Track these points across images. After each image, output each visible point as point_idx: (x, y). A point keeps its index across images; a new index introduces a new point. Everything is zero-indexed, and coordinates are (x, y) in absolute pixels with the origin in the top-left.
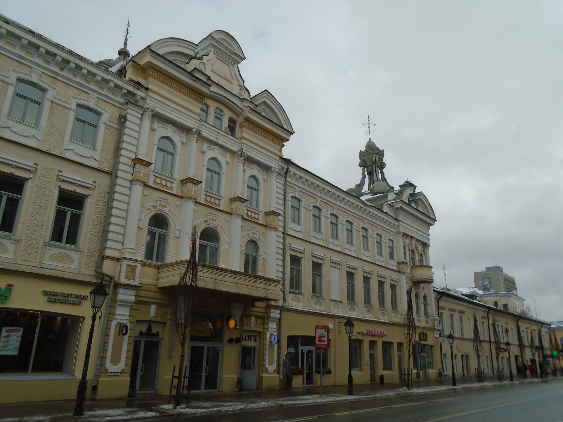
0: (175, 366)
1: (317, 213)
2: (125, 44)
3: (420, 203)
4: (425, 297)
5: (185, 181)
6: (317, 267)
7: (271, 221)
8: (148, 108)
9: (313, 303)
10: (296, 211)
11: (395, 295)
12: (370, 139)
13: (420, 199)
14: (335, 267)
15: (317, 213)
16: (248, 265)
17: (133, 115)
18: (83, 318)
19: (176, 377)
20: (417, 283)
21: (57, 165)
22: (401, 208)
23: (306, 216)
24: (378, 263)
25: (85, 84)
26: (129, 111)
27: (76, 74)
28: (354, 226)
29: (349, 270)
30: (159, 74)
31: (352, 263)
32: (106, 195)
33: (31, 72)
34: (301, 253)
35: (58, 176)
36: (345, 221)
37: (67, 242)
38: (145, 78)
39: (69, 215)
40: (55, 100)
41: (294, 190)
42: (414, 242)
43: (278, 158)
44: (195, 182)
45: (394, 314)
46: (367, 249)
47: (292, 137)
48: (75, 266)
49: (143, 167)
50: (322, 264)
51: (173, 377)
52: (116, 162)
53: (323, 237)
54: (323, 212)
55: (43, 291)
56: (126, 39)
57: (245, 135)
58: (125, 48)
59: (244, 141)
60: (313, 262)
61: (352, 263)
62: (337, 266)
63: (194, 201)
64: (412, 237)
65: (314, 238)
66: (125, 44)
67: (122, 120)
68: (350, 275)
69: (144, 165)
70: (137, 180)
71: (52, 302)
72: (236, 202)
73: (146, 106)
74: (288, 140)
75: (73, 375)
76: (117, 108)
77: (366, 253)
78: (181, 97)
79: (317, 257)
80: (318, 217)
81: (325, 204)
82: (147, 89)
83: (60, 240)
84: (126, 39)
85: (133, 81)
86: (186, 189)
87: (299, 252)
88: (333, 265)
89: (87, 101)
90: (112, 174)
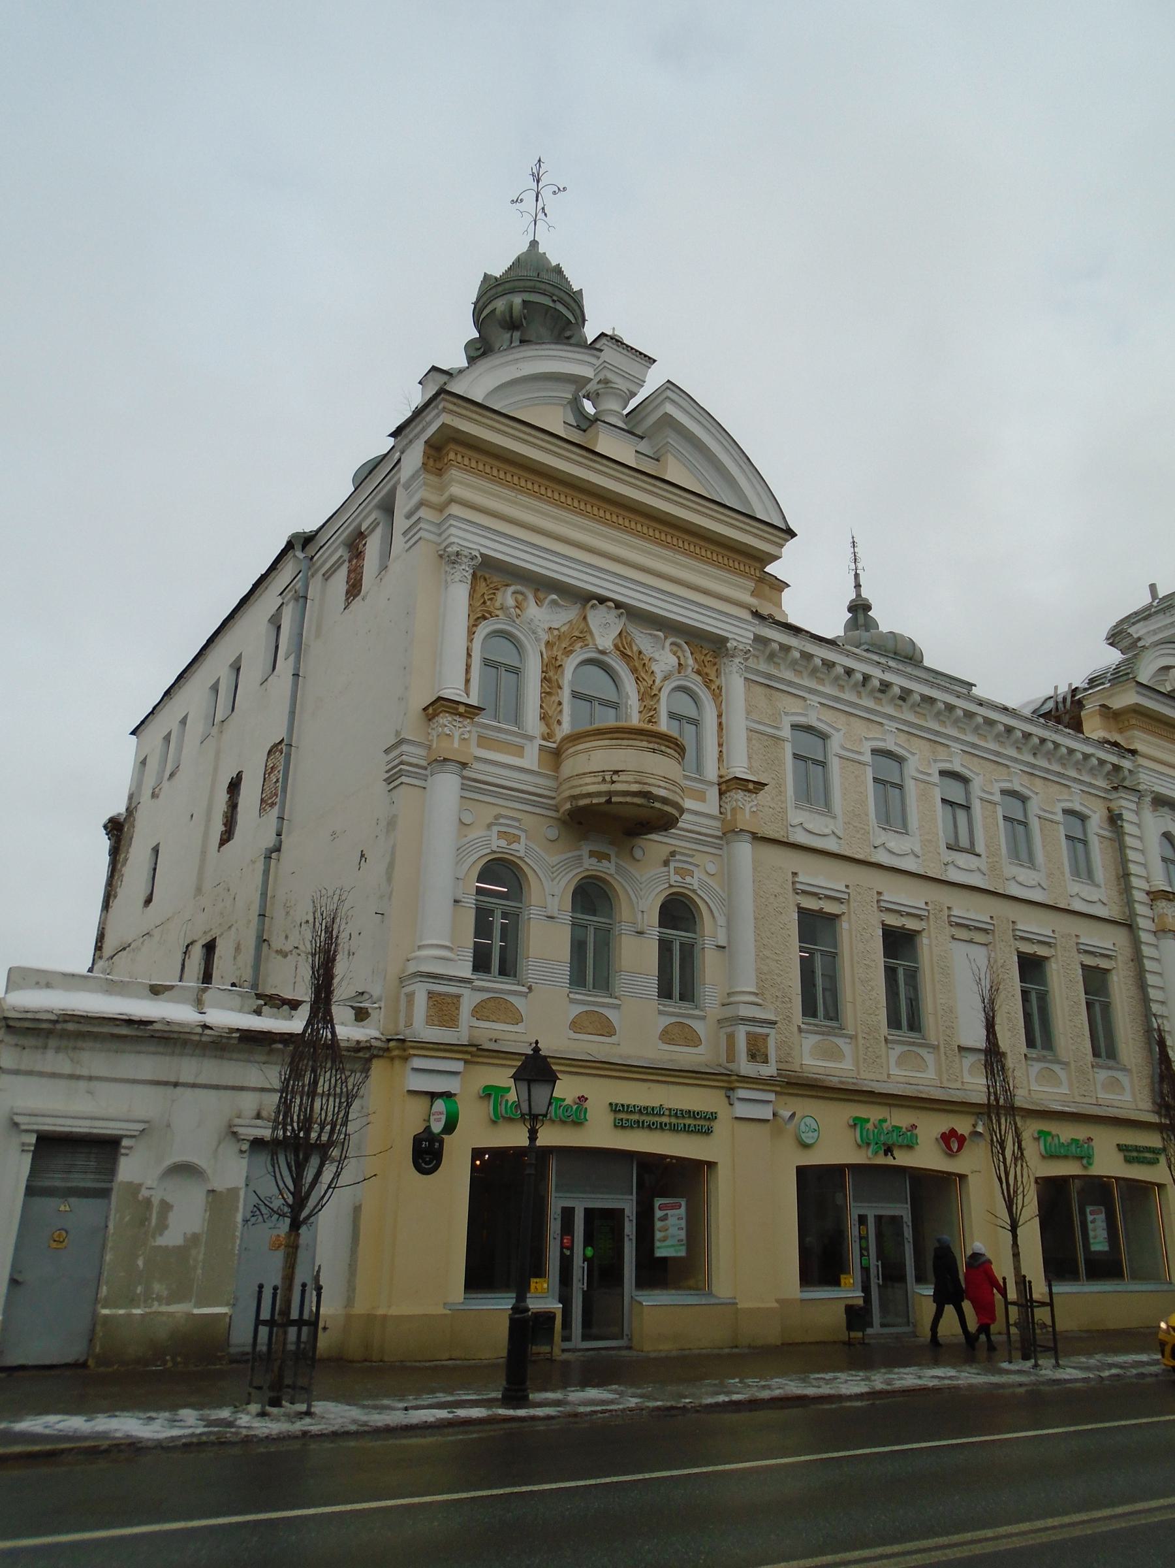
0: (261, 1287)
1: (956, 792)
2: (858, 586)
3: (673, 439)
4: (678, 912)
5: (430, 710)
6: (899, 942)
7: (733, 810)
8: (458, 554)
9: (893, 1061)
10: (961, 815)
11: (1043, 998)
12: (534, 244)
13: (668, 421)
14: (971, 941)
15: (956, 792)
16: (1039, 1008)
17: (1125, 804)
18: (711, 1165)
19: (265, 1323)
20: (616, 823)
21: (879, 881)
22: (1137, 711)
23: (851, 785)
24: (1078, 906)
25: (796, 680)
26: (1124, 803)
27: (924, 712)
28: (1034, 807)
29: (1090, 961)
30: (469, 453)
31: (1035, 924)
32: (1131, 964)
33: (1009, 774)
34: (1048, 944)
35: (1077, 944)
36: (867, 747)
37: (503, 972)
38: (1121, 731)
39: (901, 972)
40: (1042, 814)
41: (800, 702)
42: (605, 630)
43: (749, 617)
44: (462, 709)
45: (1037, 1067)
46: (1031, 863)
47: (791, 544)
48: (930, 1074)
49: (748, 797)
50: (1108, 970)
51: (258, 1322)
52: (1129, 902)
53: (837, 826)
54: (912, 766)
55: (611, 1104)
56: (857, 576)
57: (456, 490)
58: (859, 595)
59: (455, 509)
60: (1084, 967)
61: (1035, 924)
62: (979, 937)
63: (748, 837)
64: (588, 599)
65: (799, 829)
66: (858, 586)
67: (1114, 819)
68: (1031, 967)
69: (461, 715)
70: (445, 760)
71: (622, 1127)
72: (732, 794)
73: (1141, 788)
74: (777, 558)
75: (710, 1294)
76: (1099, 801)
77: (1023, 874)
78: (707, 574)
79: (967, 926)
80: (1020, 822)
81: (843, 718)
82: (1133, 752)
83: (670, 997)
84: (857, 576)
85: (1108, 742)
86: (434, 733)
87: (1040, 942)
88: (963, 934)
89: (805, 715)
90: (1129, 925)
